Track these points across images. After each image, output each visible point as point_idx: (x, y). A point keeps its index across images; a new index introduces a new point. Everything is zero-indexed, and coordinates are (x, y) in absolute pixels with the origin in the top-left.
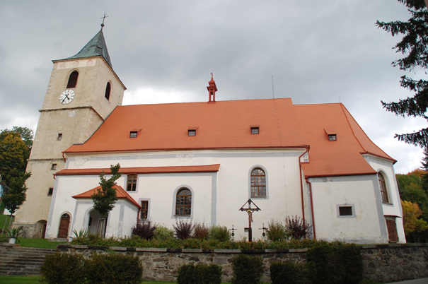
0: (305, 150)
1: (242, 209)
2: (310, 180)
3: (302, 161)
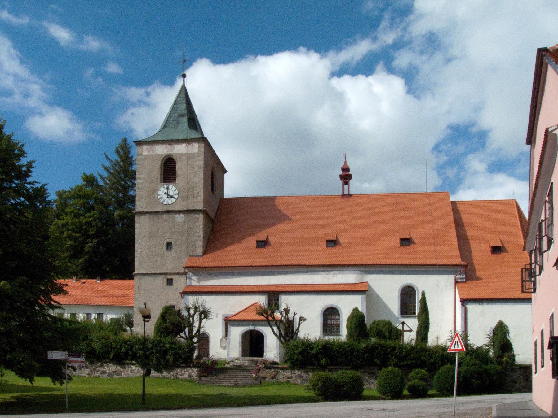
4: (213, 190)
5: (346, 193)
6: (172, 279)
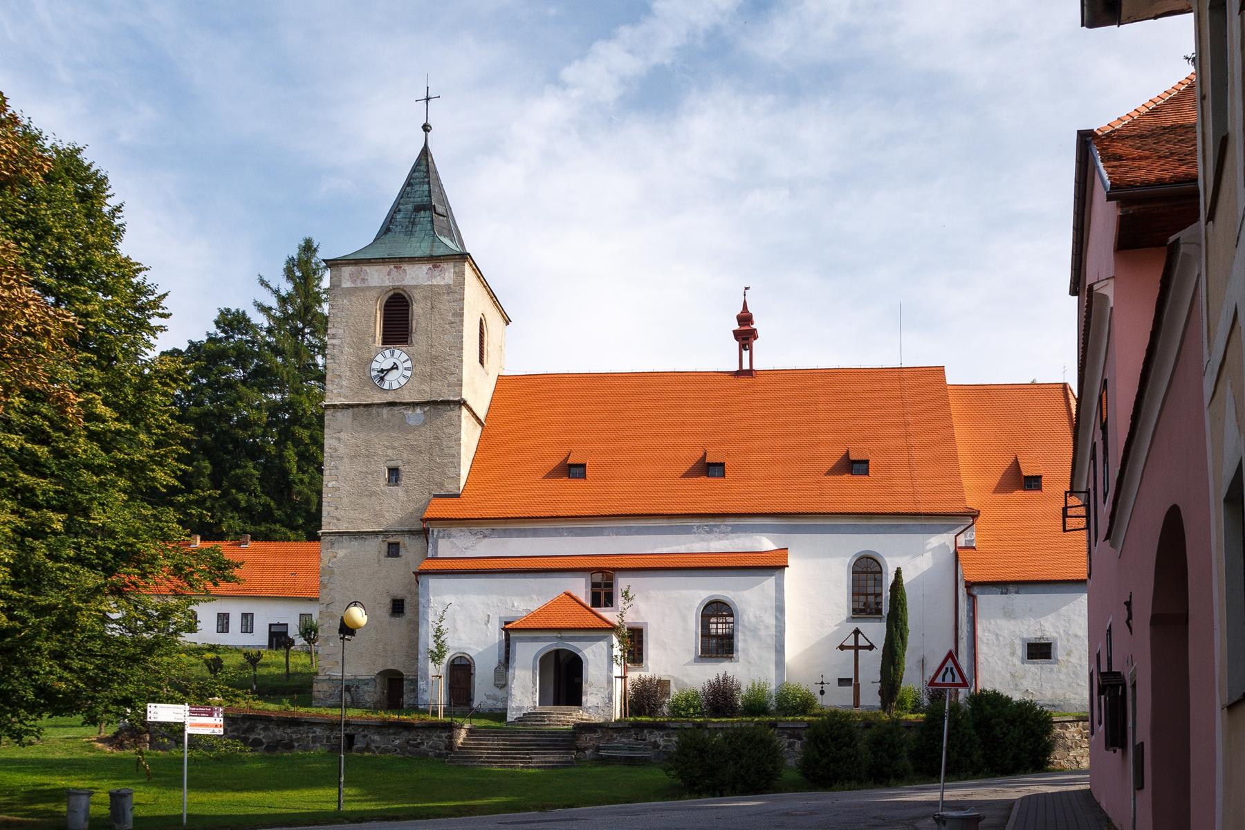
1: (842, 647)
2: (975, 591)
4: (481, 362)
5: (746, 366)
6: (398, 544)
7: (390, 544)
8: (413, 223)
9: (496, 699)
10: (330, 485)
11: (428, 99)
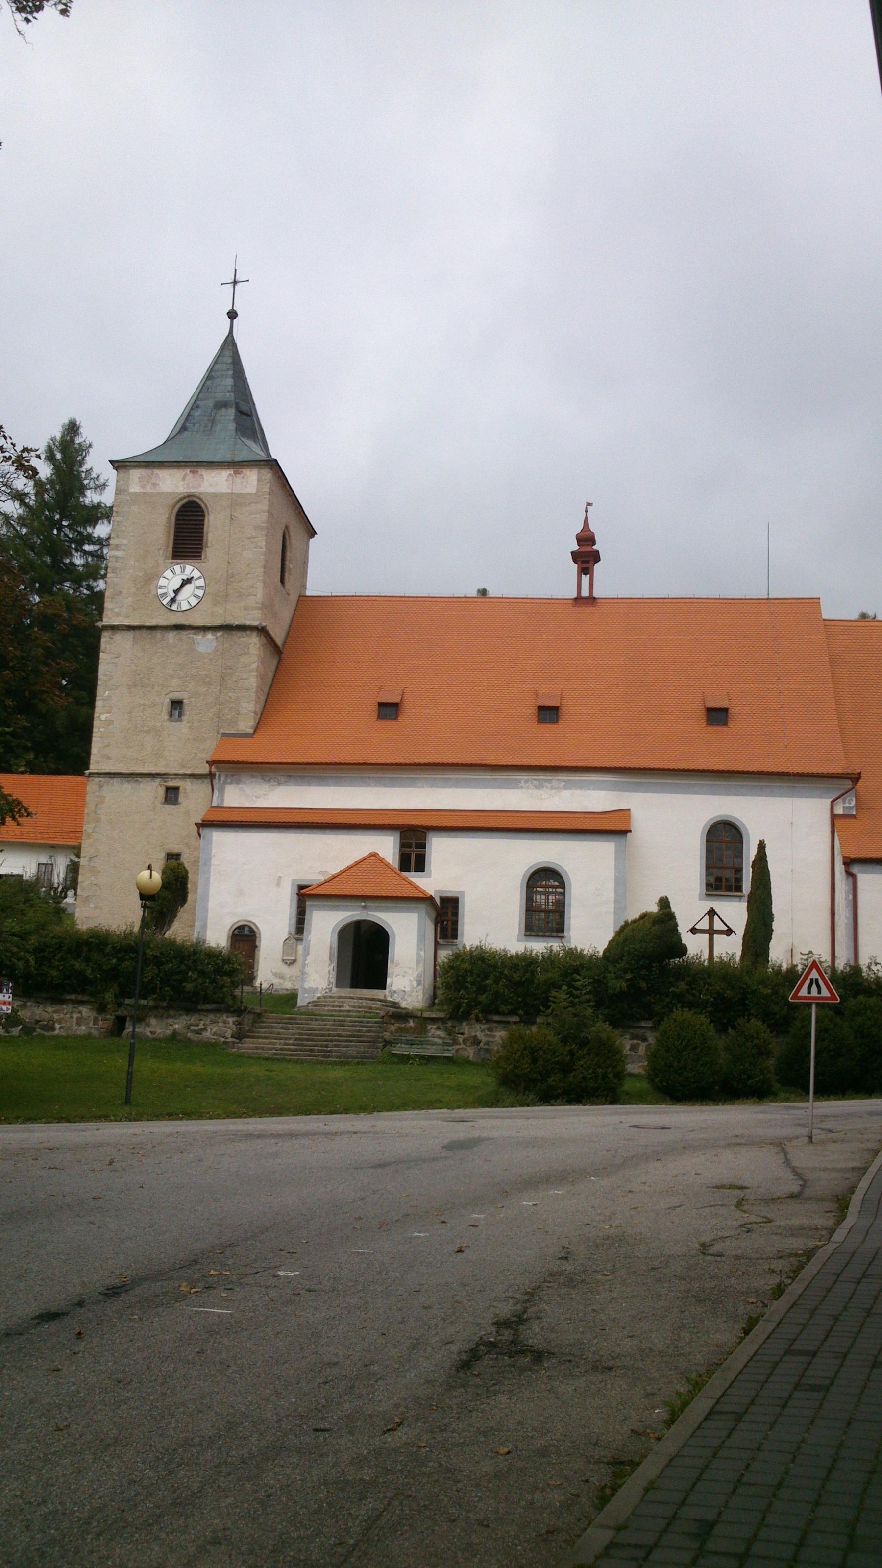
0: (848, 784)
2: (855, 869)
3: (839, 810)
4: (282, 581)
5: (585, 593)
7: (168, 789)
8: (213, 422)
9: (282, 977)
10: (103, 717)
11: (235, 283)
